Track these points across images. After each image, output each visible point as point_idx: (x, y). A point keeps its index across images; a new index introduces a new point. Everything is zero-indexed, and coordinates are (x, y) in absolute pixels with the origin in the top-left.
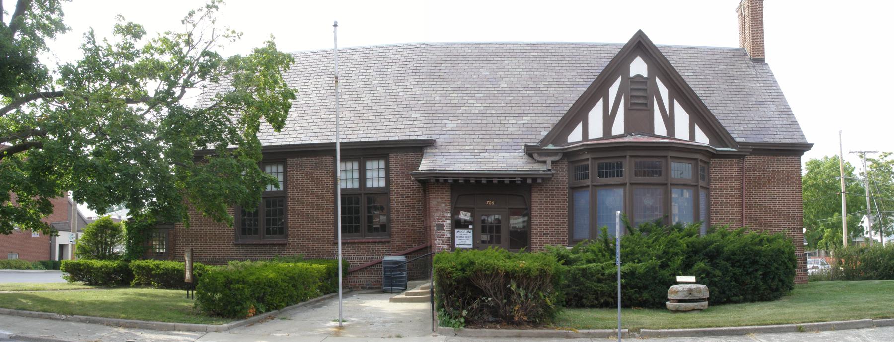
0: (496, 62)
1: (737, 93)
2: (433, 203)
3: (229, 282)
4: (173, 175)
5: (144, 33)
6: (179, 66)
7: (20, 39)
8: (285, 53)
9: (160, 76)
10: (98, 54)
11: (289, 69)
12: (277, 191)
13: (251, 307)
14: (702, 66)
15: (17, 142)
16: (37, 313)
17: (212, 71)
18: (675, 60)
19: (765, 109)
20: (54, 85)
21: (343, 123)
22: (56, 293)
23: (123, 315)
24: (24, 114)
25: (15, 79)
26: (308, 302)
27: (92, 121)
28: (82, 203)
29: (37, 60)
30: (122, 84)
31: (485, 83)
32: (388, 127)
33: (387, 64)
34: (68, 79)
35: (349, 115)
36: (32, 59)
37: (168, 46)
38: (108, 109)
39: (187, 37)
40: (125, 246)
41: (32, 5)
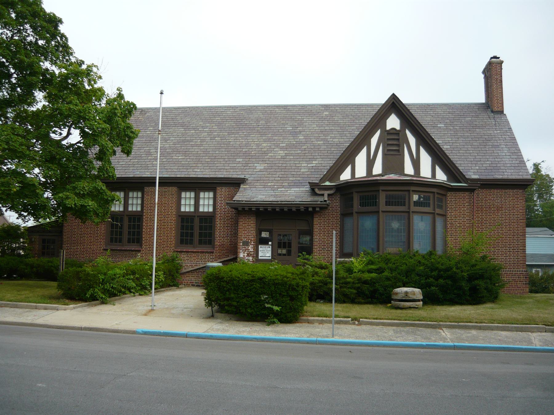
0: (297, 120)
1: (478, 139)
14: (452, 119)
18: (431, 115)
19: (499, 152)
31: (288, 135)
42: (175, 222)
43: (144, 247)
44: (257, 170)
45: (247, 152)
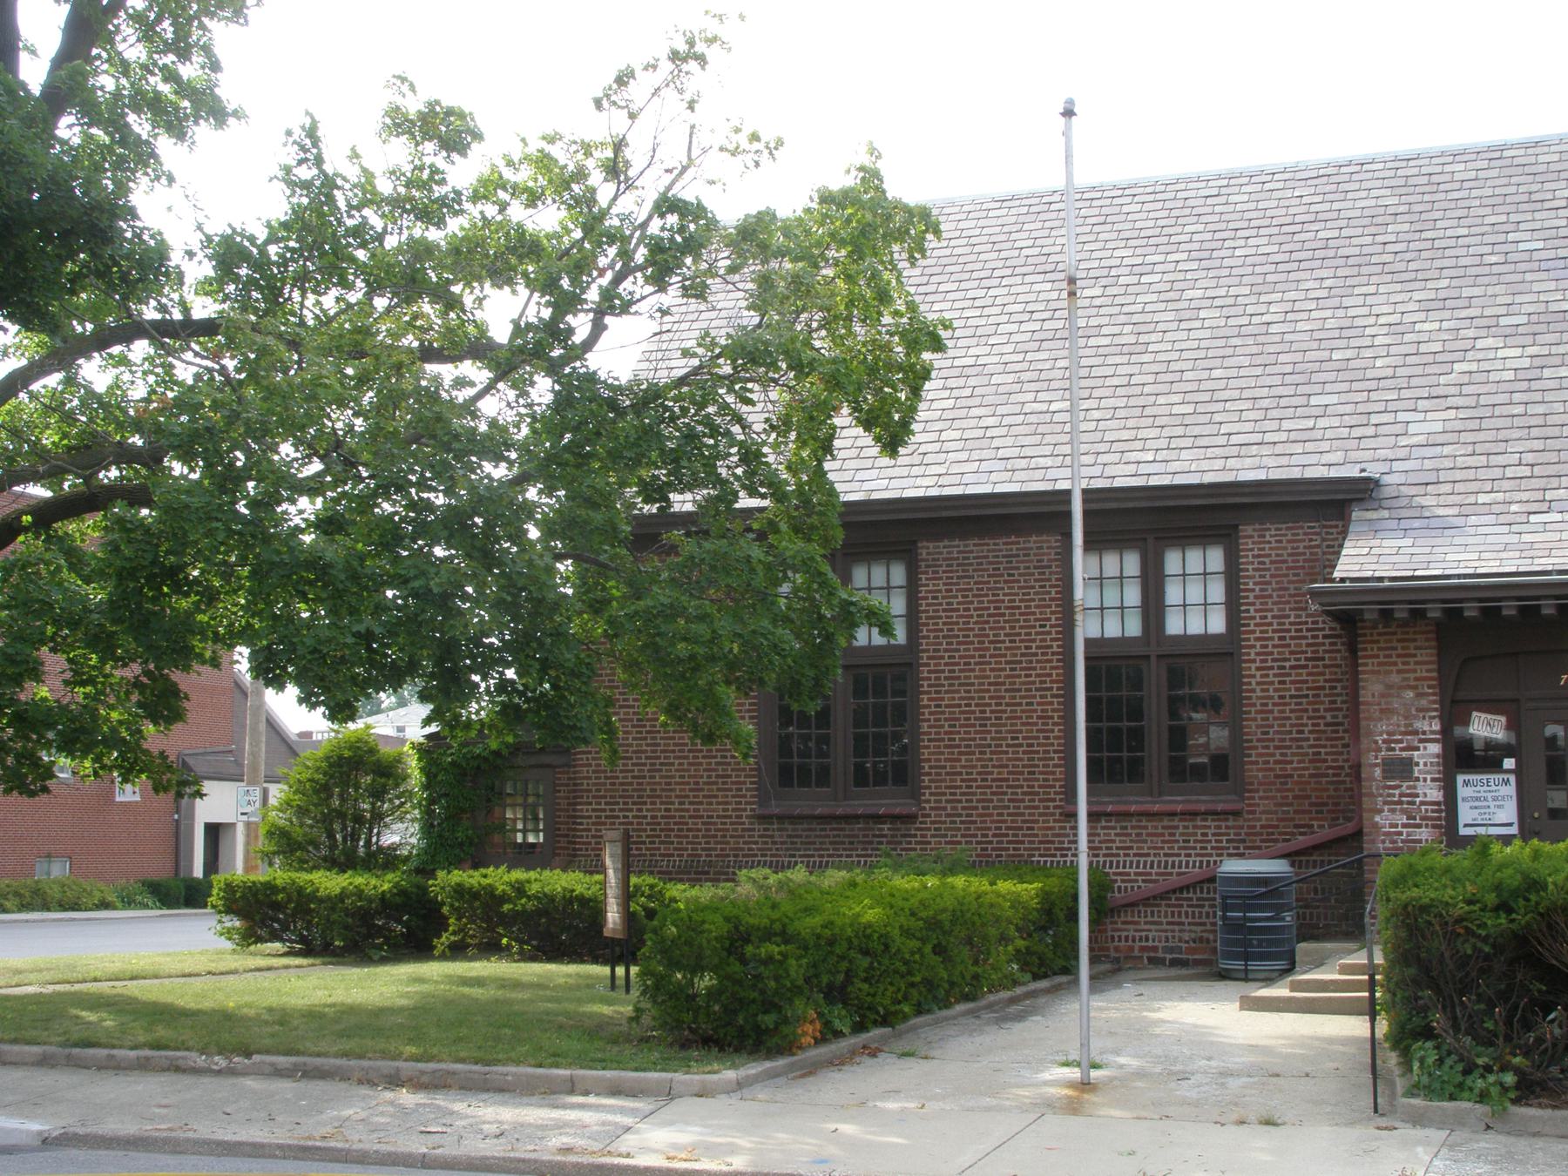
2: (1371, 688)
3: (738, 938)
4: (566, 595)
5: (478, 136)
6: (587, 245)
7: (76, 141)
8: (912, 204)
9: (525, 275)
10: (331, 199)
11: (924, 257)
12: (889, 646)
13: (806, 1015)
15: (66, 485)
16: (133, 1054)
17: (688, 261)
20: (190, 297)
21: (1092, 426)
22: (197, 984)
23: (411, 1050)
24: (91, 393)
25: (58, 272)
26: (983, 1003)
27: (315, 419)
28: (281, 687)
29: (132, 213)
30: (409, 301)
32: (1235, 439)
33: (1231, 234)
34: (236, 279)
35: (1112, 402)
36: (115, 209)
37: (550, 181)
38: (363, 380)
39: (609, 153)
40: (417, 826)
41: (117, 27)
42: (1058, 689)
43: (928, 801)
44: (1414, 440)
45: (1352, 364)
